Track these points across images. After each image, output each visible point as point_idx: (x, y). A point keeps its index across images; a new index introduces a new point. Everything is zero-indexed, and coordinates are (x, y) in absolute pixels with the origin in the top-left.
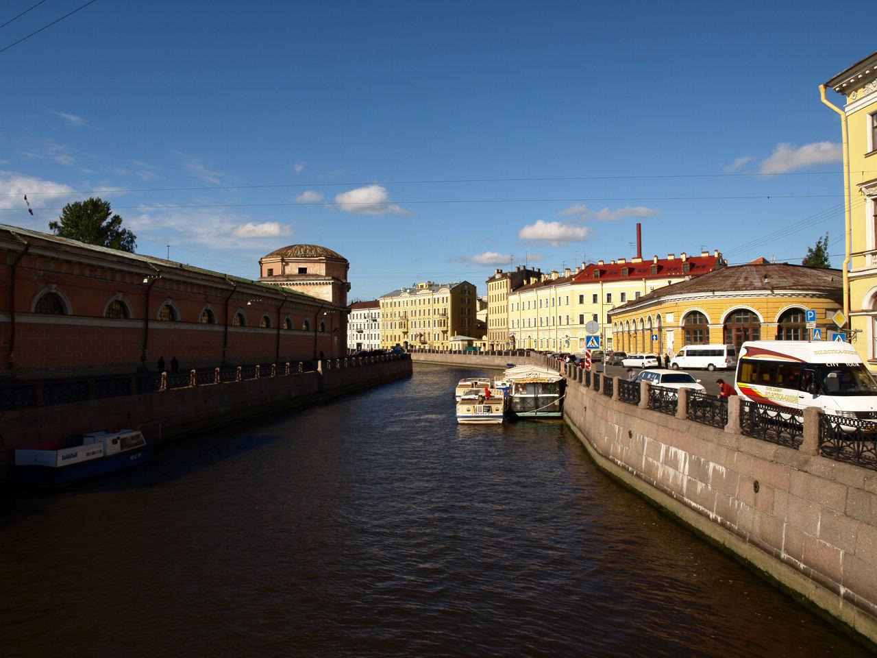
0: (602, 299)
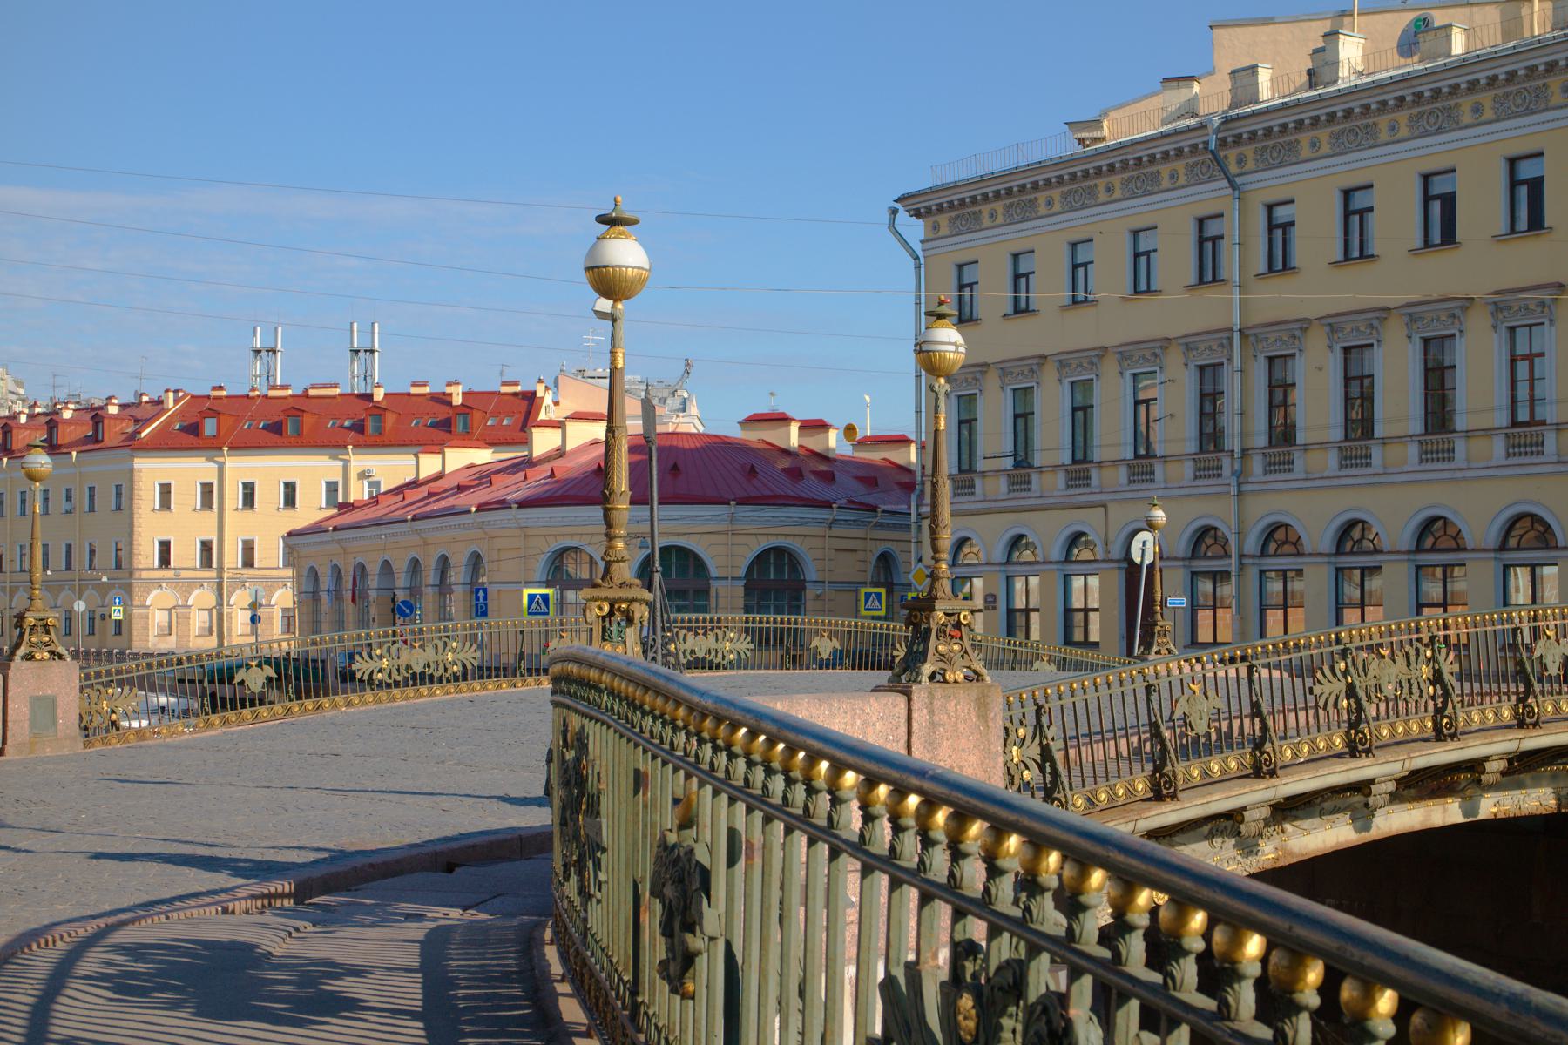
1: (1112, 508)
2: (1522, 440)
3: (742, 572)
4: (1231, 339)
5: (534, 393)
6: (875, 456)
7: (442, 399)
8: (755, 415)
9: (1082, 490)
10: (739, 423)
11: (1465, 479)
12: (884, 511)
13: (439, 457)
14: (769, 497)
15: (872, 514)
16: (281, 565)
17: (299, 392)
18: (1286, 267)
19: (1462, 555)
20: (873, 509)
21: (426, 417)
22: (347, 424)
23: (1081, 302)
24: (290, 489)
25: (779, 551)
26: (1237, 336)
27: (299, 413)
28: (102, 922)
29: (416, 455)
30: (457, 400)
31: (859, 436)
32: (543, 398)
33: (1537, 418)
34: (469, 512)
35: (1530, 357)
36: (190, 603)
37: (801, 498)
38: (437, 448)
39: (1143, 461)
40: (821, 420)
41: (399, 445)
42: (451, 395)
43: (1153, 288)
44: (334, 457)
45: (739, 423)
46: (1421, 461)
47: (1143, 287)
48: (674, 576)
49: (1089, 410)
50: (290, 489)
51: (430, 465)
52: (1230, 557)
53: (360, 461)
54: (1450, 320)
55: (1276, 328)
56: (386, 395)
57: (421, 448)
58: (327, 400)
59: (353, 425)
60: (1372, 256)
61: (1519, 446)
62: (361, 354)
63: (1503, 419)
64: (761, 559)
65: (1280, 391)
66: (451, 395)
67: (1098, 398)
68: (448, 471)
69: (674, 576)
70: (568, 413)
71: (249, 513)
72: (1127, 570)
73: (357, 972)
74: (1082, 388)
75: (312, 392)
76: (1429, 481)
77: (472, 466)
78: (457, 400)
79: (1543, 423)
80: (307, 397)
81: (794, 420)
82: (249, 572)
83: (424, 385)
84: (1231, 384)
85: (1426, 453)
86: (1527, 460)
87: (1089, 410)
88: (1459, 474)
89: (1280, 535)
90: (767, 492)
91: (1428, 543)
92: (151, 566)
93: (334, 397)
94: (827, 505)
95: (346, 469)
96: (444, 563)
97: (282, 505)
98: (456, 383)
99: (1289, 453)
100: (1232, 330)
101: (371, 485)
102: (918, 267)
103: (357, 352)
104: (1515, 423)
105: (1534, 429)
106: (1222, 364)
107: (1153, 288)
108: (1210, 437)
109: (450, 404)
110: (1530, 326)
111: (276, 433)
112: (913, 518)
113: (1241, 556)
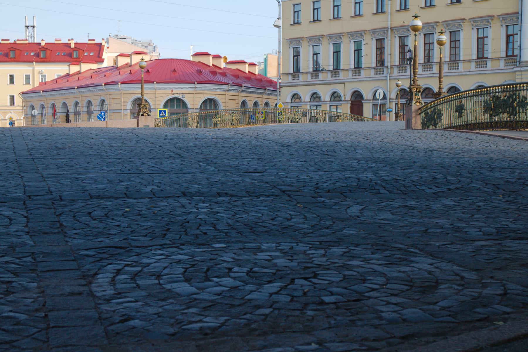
0: (19, 80)
1: (346, 83)
2: (514, 61)
3: (199, 107)
4: (388, 31)
5: (101, 44)
6: (234, 67)
7: (68, 45)
8: (197, 53)
9: (336, 78)
10: (192, 56)
11: (462, 75)
12: (244, 87)
13: (79, 66)
14: (207, 81)
15: (240, 87)
16: (9, 105)
17: (13, 42)
18: (405, 8)
19: (341, 102)
20: (241, 86)
21: (62, 52)
22: (32, 54)
23: (358, 15)
24: (12, 77)
25: (210, 100)
26: (390, 30)
27: (15, 50)
28: (399, 263)
29: (69, 66)
30: (73, 46)
31: (228, 61)
32: (104, 46)
33: (485, 56)
34: (102, 85)
35: (513, 35)
36: (6, 118)
37: (217, 82)
38: (78, 63)
39: (317, 70)
40: (219, 55)
41: (53, 62)
42: (70, 44)
43: (339, 17)
44: (29, 66)
45: (192, 56)
46: (375, 74)
47: (358, 13)
48: (175, 108)
49: (339, 53)
50: (12, 77)
51: (74, 69)
52: (386, 99)
53: (39, 67)
54: (459, 26)
55: (402, 28)
56: (46, 43)
57: (70, 63)
58: (23, 45)
59: (35, 54)
60: (434, 5)
61: (513, 63)
62: (30, 28)
63: (503, 55)
64: (205, 102)
65: (380, 50)
66: (70, 44)
67: (302, 51)
68: (82, 71)
69: (175, 108)
70: (132, 51)
71: (12, 85)
72: (351, 103)
73: (433, 272)
74: (380, 41)
75: (18, 42)
76: (462, 75)
77: (91, 70)
78: (73, 46)
79: (487, 58)
80: (16, 44)
81: (210, 55)
82: (12, 108)
83: (60, 40)
84: (387, 45)
85: (507, 63)
86: (482, 69)
87: (318, 55)
88: (460, 74)
89: (335, 95)
90: (206, 80)
91: (293, 101)
92: (7, 105)
93: (26, 44)
94: (227, 84)
95: (33, 70)
96: (89, 103)
97: (9, 83)
98: (72, 40)
99: (360, 70)
100: (388, 28)
101: (42, 76)
102: (279, 5)
103: (28, 27)
104: (507, 56)
105: (484, 60)
106: (384, 39)
107: (361, 14)
108: (381, 62)
109: (70, 47)
110: (484, 28)
111: (6, 57)
112: (278, 87)
113: (390, 99)
